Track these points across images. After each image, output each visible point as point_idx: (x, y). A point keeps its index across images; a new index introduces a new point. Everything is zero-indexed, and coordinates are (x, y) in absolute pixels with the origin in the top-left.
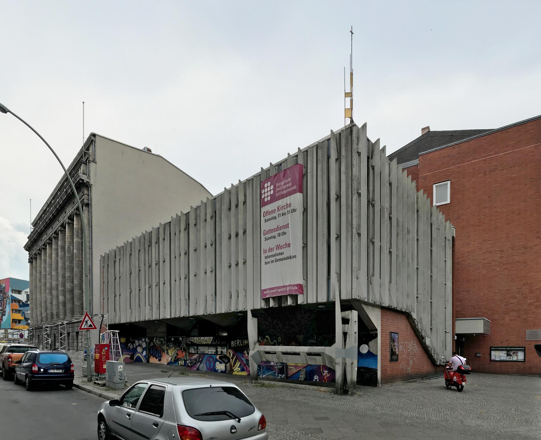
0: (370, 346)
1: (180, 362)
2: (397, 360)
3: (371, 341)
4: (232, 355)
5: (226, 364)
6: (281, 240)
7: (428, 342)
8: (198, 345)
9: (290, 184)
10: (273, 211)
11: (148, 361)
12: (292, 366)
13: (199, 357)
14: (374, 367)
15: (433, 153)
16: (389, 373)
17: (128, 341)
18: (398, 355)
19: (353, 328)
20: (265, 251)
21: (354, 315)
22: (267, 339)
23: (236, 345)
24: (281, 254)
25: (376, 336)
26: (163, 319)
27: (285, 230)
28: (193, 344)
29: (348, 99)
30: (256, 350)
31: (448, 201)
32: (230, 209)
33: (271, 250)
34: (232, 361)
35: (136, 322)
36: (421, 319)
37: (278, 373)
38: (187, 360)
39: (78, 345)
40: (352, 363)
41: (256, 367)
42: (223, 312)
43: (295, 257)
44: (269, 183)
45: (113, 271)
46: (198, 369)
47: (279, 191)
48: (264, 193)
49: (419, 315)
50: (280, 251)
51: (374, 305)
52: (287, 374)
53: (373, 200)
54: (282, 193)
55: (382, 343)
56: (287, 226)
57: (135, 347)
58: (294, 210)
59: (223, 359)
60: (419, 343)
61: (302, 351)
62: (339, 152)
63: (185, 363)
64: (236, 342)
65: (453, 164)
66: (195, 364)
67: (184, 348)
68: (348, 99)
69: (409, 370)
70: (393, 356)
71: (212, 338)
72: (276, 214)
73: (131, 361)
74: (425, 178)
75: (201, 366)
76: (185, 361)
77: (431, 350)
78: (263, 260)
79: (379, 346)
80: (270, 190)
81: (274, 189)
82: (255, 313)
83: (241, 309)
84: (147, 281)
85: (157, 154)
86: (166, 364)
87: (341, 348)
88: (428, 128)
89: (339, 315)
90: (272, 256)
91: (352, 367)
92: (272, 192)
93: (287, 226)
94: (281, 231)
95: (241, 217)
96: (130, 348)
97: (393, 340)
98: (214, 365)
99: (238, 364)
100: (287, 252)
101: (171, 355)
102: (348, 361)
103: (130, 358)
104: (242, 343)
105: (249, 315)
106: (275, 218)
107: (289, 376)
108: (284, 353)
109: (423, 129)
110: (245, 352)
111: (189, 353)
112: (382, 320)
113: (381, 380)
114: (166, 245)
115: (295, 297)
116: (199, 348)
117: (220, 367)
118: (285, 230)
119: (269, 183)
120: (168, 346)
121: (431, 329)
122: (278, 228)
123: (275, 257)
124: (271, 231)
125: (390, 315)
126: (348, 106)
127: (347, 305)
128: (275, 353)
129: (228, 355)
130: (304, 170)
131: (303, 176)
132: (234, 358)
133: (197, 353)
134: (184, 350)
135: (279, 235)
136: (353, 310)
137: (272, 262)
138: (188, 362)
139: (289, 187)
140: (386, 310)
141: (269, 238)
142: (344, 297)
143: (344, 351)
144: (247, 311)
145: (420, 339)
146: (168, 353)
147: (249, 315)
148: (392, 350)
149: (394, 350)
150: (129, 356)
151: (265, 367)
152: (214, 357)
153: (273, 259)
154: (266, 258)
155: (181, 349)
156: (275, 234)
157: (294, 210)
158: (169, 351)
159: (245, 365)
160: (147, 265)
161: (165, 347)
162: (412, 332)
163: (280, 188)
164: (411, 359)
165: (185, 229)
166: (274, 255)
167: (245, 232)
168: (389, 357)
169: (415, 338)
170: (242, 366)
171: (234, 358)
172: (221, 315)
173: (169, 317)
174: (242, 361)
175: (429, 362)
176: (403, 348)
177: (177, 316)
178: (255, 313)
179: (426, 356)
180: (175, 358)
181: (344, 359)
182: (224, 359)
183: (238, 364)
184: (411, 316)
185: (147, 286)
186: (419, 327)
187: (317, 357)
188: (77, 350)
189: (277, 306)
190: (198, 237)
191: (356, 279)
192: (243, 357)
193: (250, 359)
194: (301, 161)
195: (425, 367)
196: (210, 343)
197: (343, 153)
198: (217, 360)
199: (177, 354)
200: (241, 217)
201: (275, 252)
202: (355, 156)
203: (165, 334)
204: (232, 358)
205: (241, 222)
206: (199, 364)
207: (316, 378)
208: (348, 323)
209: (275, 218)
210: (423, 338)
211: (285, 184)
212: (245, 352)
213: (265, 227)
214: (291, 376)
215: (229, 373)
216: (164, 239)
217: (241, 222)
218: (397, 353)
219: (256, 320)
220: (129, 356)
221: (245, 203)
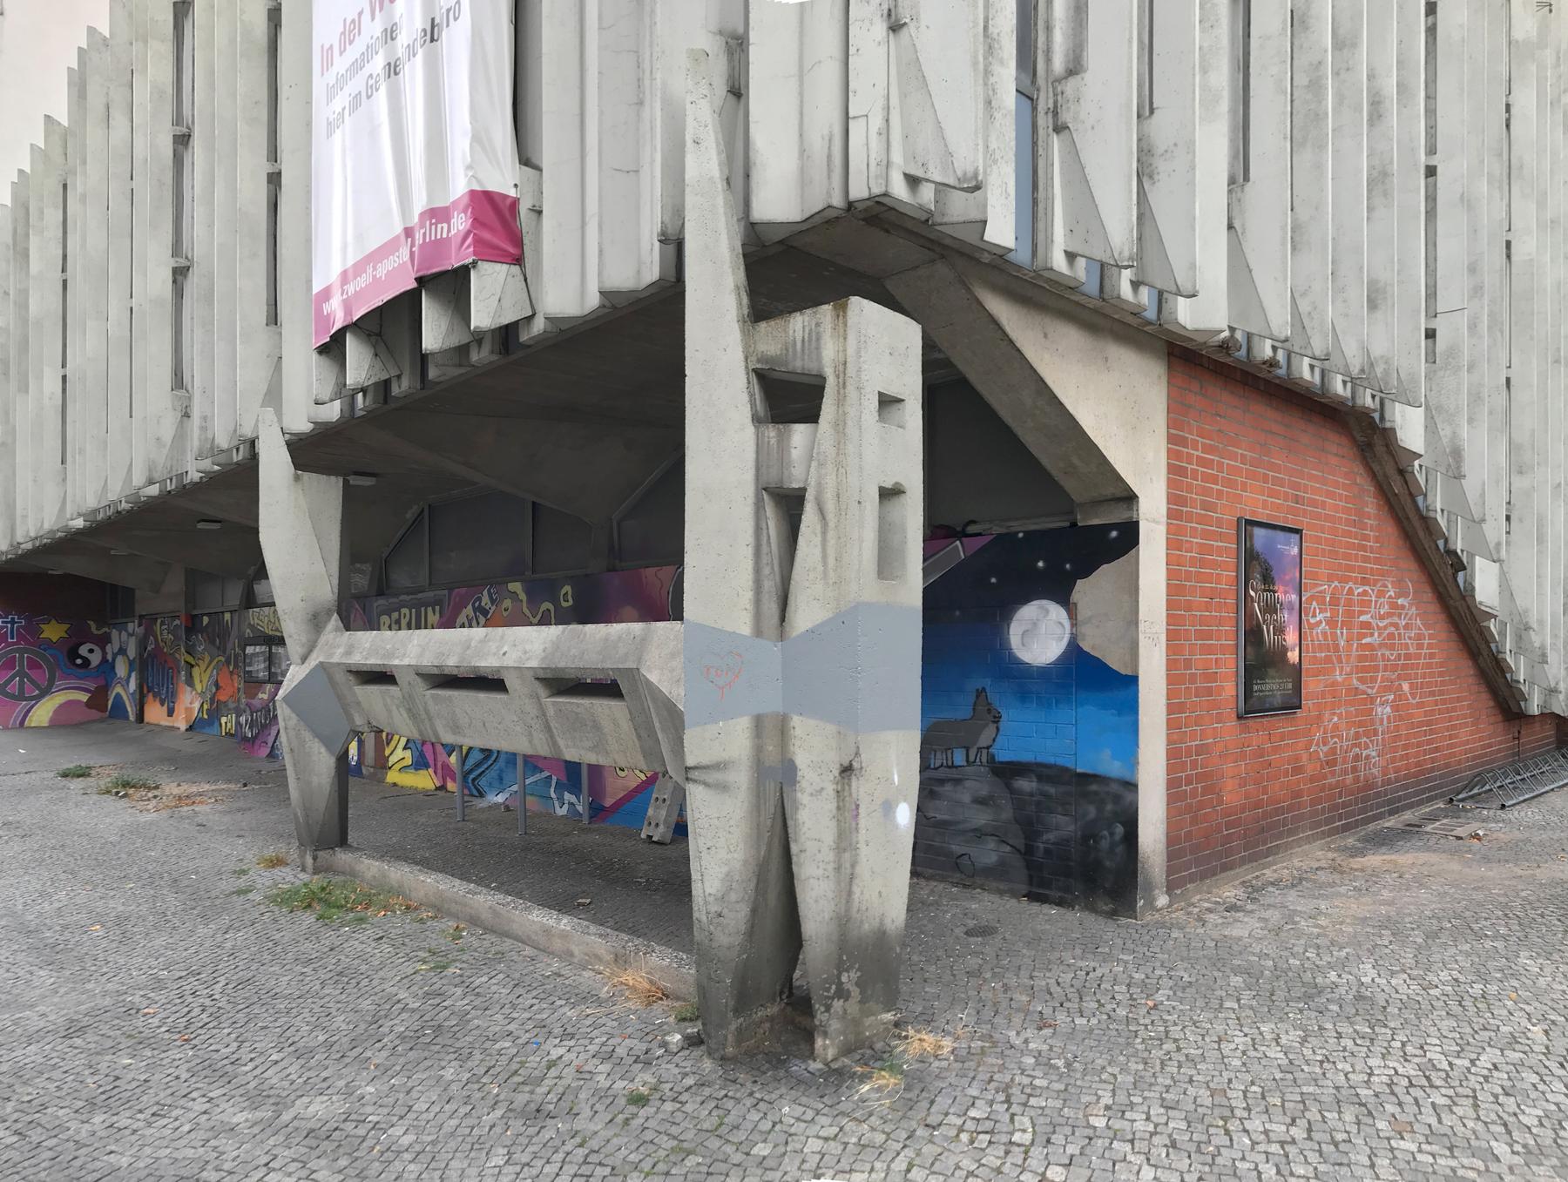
0: (1083, 612)
1: (224, 720)
2: (1292, 704)
3: (1086, 573)
7: (1485, 585)
11: (140, 718)
14: (1110, 766)
16: (1232, 795)
18: (1298, 669)
19: (874, 448)
21: (875, 350)
25: (1129, 536)
30: (312, 662)
36: (1457, 453)
37: (560, 787)
41: (323, 764)
49: (1445, 432)
55: (1174, 591)
60: (1428, 595)
61: (510, 661)
69: (1375, 760)
70: (1266, 679)
73: (95, 714)
77: (1503, 633)
79: (1148, 609)
86: (183, 727)
91: (846, 812)
96: (87, 662)
97: (1257, 568)
102: (813, 750)
103: (89, 704)
105: (275, 465)
112: (1171, 439)
113: (1172, 855)
121: (1508, 518)
125: (1242, 425)
127: (794, 268)
136: (856, 302)
140: (1214, 373)
143: (771, 650)
145: (1439, 570)
147: (275, 465)
148: (1253, 635)
149: (1268, 635)
150: (84, 697)
155: (228, 662)
161: (184, 657)
162: (1390, 529)
164: (1387, 689)
168: (1230, 690)
169: (1410, 565)
175: (1485, 701)
176: (1331, 623)
178: (309, 452)
179: (1467, 668)
180: (212, 699)
181: (772, 732)
184: (1387, 436)
186: (1437, 502)
187: (602, 707)
191: (880, 28)
193: (283, 711)
195: (1464, 734)
199: (217, 685)
208: (812, 417)
210: (1459, 565)
214: (619, 804)
215: (372, 777)
218: (1293, 656)
219: (328, 491)
220: (84, 697)
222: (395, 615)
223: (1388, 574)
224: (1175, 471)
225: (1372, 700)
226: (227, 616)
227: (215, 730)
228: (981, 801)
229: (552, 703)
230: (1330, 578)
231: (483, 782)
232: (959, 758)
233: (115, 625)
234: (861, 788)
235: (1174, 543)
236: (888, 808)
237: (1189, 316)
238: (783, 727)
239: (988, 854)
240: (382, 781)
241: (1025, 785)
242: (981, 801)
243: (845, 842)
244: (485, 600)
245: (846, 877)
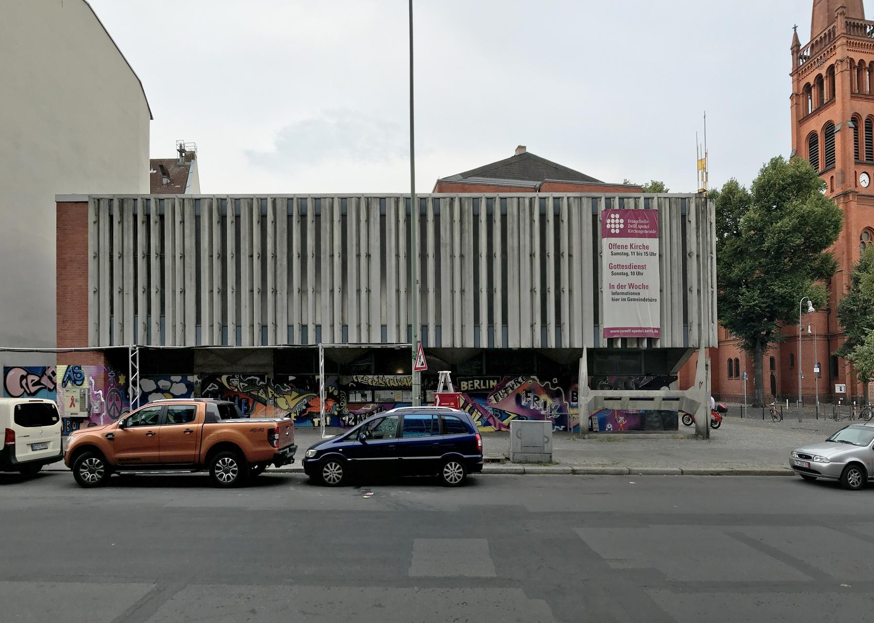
8: (373, 389)
22: (534, 380)
24: (639, 294)
27: (641, 271)
43: (656, 300)
64: (473, 384)
72: (629, 250)
81: (625, 223)
83: (577, 345)
85: (621, 182)
88: (525, 147)
90: (623, 293)
100: (644, 294)
104: (485, 384)
106: (627, 254)
108: (631, 399)
109: (519, 147)
110: (492, 397)
115: (651, 341)
116: (377, 392)
120: (276, 390)
128: (620, 399)
133: (373, 402)
135: (633, 273)
137: (624, 300)
146: (276, 405)
153: (626, 297)
156: (628, 271)
159: (491, 416)
166: (627, 294)
170: (485, 418)
174: (486, 411)
192: (487, 405)
199: (308, 405)
201: (627, 290)
202: (709, 224)
203: (270, 369)
207: (609, 426)
209: (627, 254)
212: (492, 397)
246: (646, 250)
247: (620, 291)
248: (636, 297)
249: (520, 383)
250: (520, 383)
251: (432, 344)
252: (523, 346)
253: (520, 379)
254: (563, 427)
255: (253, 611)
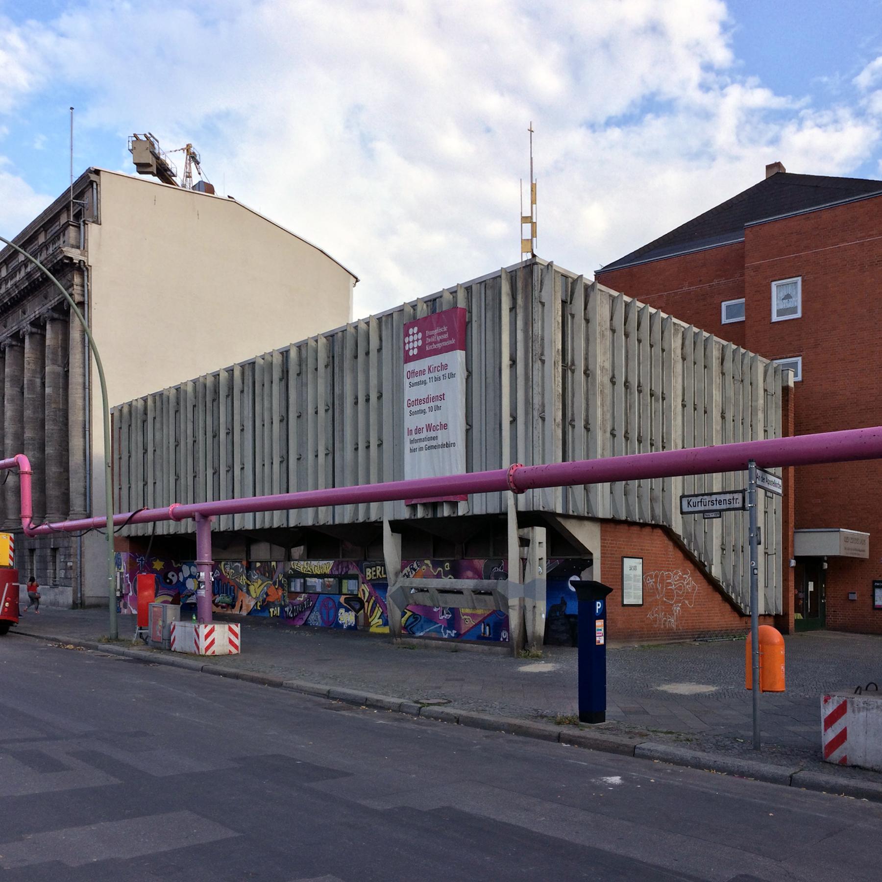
1: (272, 610)
4: (367, 594)
5: (357, 611)
6: (432, 418)
8: (304, 576)
9: (446, 336)
10: (422, 372)
12: (467, 615)
13: (309, 599)
15: (773, 225)
17: (168, 568)
20: (410, 432)
21: (540, 534)
22: (427, 565)
23: (375, 575)
26: (240, 531)
28: (298, 574)
29: (527, 227)
30: (398, 585)
31: (799, 315)
32: (356, 357)
33: (418, 431)
34: (368, 607)
35: (187, 534)
37: (445, 629)
38: (285, 606)
39: (55, 573)
40: (534, 607)
42: (346, 522)
44: (416, 329)
45: (140, 439)
46: (306, 624)
47: (431, 344)
48: (409, 343)
50: (432, 434)
51: (580, 518)
52: (458, 629)
53: (573, 364)
54: (435, 346)
56: (442, 397)
57: (181, 579)
58: (452, 375)
59: (352, 603)
62: (514, 298)
63: (282, 610)
64: (375, 571)
65: (807, 248)
66: (301, 612)
67: (280, 582)
68: (527, 227)
71: (332, 562)
74: (756, 269)
75: (312, 617)
76: (282, 608)
78: (407, 446)
80: (418, 340)
81: (424, 339)
82: (396, 526)
83: (373, 518)
84: (209, 457)
87: (517, 582)
89: (513, 533)
92: (420, 343)
93: (442, 397)
94: (432, 404)
95: (373, 373)
96: (171, 581)
98: (336, 616)
99: (378, 612)
100: (442, 437)
101: (254, 595)
102: (529, 603)
105: (387, 528)
106: (425, 383)
107: (463, 632)
111: (290, 592)
114: (246, 401)
117: (347, 618)
118: (438, 403)
119: (416, 329)
122: (426, 400)
123: (425, 443)
124: (419, 402)
126: (527, 235)
128: (427, 591)
129: (360, 595)
130: (467, 315)
131: (466, 325)
132: (372, 602)
134: (281, 585)
135: (431, 409)
138: (287, 609)
139: (445, 340)
141: (416, 413)
142: (522, 508)
144: (382, 522)
146: (248, 592)
147: (387, 528)
151: (422, 616)
152: (335, 598)
154: (412, 442)
157: (452, 375)
158: (252, 588)
160: (210, 434)
163: (433, 339)
165: (281, 380)
167: (380, 397)
171: (372, 602)
172: (342, 526)
173: (251, 527)
177: (267, 526)
178: (396, 526)
180: (264, 601)
181: (522, 600)
182: (355, 603)
183: (378, 612)
185: (210, 472)
187: (487, 597)
188: (55, 586)
189: (429, 516)
190: (304, 394)
194: (461, 304)
196: (328, 571)
197: (520, 301)
198: (341, 606)
200: (373, 373)
204: (368, 601)
205: (373, 382)
206: (307, 613)
209: (425, 383)
211: (439, 334)
213: (410, 393)
214: (465, 633)
216: (242, 392)
217: (373, 382)
219: (399, 537)
221: (380, 350)
222: (374, 569)
223: (678, 568)
224: (603, 547)
225: (672, 605)
226: (274, 563)
227: (266, 614)
228: (562, 624)
229: (474, 597)
230: (654, 570)
231: (414, 629)
232: (558, 614)
233: (185, 563)
234: (537, 610)
235: (603, 563)
236: (541, 615)
237: (601, 516)
238: (524, 600)
239: (564, 637)
240: (368, 631)
241: (572, 620)
242: (562, 624)
243: (534, 619)
244: (415, 566)
245: (534, 626)
246: (443, 372)
247: (417, 437)
248: (434, 443)
249: (415, 570)
250: (415, 570)
251: (747, 472)
252: (304, 524)
253: (415, 566)
254: (454, 632)
255: (72, 108)
